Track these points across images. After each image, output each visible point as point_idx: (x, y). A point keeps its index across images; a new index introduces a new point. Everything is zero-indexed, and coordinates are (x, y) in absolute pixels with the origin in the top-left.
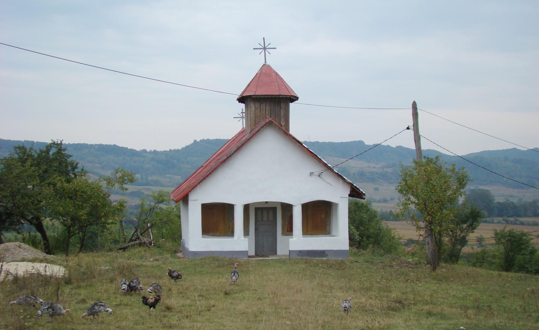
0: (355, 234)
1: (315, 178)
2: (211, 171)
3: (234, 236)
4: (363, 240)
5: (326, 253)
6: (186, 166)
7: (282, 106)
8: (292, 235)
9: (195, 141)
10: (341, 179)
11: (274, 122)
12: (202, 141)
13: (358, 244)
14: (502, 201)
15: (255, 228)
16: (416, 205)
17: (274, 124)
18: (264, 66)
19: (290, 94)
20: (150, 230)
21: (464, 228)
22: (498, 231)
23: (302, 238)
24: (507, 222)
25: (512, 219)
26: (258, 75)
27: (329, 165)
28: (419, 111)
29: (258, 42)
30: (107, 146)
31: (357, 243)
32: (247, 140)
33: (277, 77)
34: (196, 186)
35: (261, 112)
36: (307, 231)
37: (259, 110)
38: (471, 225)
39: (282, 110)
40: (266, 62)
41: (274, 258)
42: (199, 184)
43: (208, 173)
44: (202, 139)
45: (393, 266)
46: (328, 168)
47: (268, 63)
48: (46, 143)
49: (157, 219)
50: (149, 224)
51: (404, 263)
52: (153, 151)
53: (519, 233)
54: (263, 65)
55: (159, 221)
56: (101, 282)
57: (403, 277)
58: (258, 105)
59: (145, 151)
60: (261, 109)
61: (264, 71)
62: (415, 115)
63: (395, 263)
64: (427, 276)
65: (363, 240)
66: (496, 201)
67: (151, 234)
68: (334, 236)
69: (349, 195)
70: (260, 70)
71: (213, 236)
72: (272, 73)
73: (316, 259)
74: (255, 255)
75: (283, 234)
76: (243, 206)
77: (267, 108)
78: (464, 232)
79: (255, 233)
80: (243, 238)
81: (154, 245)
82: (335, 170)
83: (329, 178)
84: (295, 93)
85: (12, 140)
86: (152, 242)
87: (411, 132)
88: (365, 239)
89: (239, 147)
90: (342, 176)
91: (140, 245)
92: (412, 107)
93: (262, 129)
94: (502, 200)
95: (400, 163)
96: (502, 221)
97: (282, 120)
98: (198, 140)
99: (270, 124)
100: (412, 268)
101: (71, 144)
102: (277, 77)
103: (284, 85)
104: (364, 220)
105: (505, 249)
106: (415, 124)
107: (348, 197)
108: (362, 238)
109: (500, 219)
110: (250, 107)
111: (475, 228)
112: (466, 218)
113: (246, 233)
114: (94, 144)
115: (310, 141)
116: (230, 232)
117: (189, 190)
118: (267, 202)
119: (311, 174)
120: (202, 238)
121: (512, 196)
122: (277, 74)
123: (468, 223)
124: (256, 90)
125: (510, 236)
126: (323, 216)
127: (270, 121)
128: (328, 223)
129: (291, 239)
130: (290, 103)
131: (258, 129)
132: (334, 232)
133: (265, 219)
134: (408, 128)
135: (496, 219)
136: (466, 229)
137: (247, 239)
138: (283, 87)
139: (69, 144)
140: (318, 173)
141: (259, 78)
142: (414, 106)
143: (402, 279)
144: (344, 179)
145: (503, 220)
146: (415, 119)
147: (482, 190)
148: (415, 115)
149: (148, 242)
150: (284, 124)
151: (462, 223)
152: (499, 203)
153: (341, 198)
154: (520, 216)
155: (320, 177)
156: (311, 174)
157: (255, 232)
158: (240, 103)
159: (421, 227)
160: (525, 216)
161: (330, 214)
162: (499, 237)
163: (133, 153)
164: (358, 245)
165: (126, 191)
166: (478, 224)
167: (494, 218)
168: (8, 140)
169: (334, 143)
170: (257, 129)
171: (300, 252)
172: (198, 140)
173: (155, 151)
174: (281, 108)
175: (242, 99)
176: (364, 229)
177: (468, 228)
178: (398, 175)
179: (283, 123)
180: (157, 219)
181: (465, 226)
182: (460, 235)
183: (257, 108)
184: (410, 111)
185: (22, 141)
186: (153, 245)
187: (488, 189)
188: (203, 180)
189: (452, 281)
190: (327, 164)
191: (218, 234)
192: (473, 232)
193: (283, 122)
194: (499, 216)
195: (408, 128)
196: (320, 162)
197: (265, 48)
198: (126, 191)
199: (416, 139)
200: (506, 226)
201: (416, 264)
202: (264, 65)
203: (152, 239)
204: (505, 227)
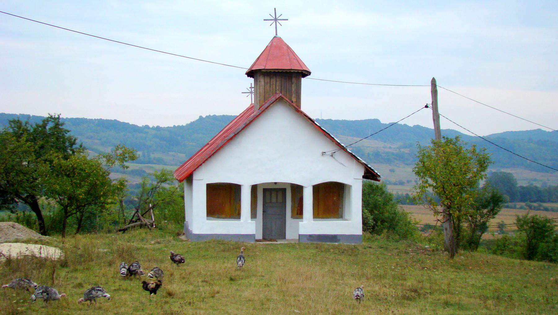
1: (327, 158)
5: (338, 238)
6: (191, 144)
8: (302, 218)
9: (201, 117)
12: (209, 117)
14: (525, 185)
15: (263, 210)
17: (285, 101)
19: (302, 68)
22: (521, 217)
24: (530, 207)
25: (535, 204)
26: (268, 48)
27: (342, 145)
28: (438, 88)
29: (268, 13)
30: (107, 120)
32: (255, 117)
33: (289, 50)
34: (201, 165)
35: (271, 87)
36: (318, 214)
37: (269, 84)
38: (492, 210)
39: (293, 85)
40: (276, 35)
42: (204, 162)
44: (208, 115)
47: (279, 35)
49: (160, 199)
50: (150, 204)
52: (156, 127)
55: (161, 202)
58: (267, 79)
59: (147, 127)
60: (271, 84)
61: (275, 44)
62: (434, 92)
63: (410, 250)
66: (518, 185)
68: (346, 220)
70: (270, 43)
71: (218, 218)
72: (283, 46)
73: (327, 244)
75: (293, 217)
76: (251, 187)
79: (263, 216)
80: (249, 220)
81: (155, 227)
82: (348, 150)
83: (341, 157)
87: (430, 111)
90: (356, 156)
91: (141, 226)
93: (272, 105)
94: (524, 184)
96: (525, 207)
97: (293, 96)
98: (204, 117)
102: (289, 50)
103: (294, 58)
105: (528, 236)
108: (377, 222)
109: (523, 204)
111: (496, 214)
112: (487, 203)
113: (254, 215)
116: (236, 214)
117: (194, 169)
118: (276, 183)
119: (323, 153)
120: (207, 220)
121: (535, 180)
122: (288, 47)
123: (489, 208)
124: (266, 64)
125: (533, 222)
127: (281, 96)
128: (340, 206)
129: (300, 223)
133: (274, 200)
134: (426, 107)
136: (486, 214)
138: (295, 61)
139: (67, 118)
140: (330, 153)
141: (269, 51)
142: (434, 83)
144: (358, 159)
145: (526, 205)
148: (434, 92)
149: (149, 224)
151: (483, 208)
152: (522, 187)
154: (544, 201)
156: (323, 153)
157: (263, 214)
158: (249, 77)
160: (549, 201)
161: (342, 197)
162: (521, 223)
163: (134, 128)
170: (266, 105)
172: (204, 117)
173: (158, 127)
174: (292, 83)
175: (251, 74)
176: (378, 213)
177: (488, 213)
178: (416, 156)
179: (294, 100)
180: (160, 199)
181: (485, 211)
182: (480, 221)
183: (267, 83)
184: (429, 89)
186: (154, 226)
187: (511, 172)
188: (208, 158)
189: (471, 269)
191: (224, 216)
192: (494, 218)
194: (522, 200)
195: (426, 107)
196: (333, 141)
197: (276, 20)
199: (435, 118)
201: (433, 251)
202: (275, 37)
203: (153, 220)
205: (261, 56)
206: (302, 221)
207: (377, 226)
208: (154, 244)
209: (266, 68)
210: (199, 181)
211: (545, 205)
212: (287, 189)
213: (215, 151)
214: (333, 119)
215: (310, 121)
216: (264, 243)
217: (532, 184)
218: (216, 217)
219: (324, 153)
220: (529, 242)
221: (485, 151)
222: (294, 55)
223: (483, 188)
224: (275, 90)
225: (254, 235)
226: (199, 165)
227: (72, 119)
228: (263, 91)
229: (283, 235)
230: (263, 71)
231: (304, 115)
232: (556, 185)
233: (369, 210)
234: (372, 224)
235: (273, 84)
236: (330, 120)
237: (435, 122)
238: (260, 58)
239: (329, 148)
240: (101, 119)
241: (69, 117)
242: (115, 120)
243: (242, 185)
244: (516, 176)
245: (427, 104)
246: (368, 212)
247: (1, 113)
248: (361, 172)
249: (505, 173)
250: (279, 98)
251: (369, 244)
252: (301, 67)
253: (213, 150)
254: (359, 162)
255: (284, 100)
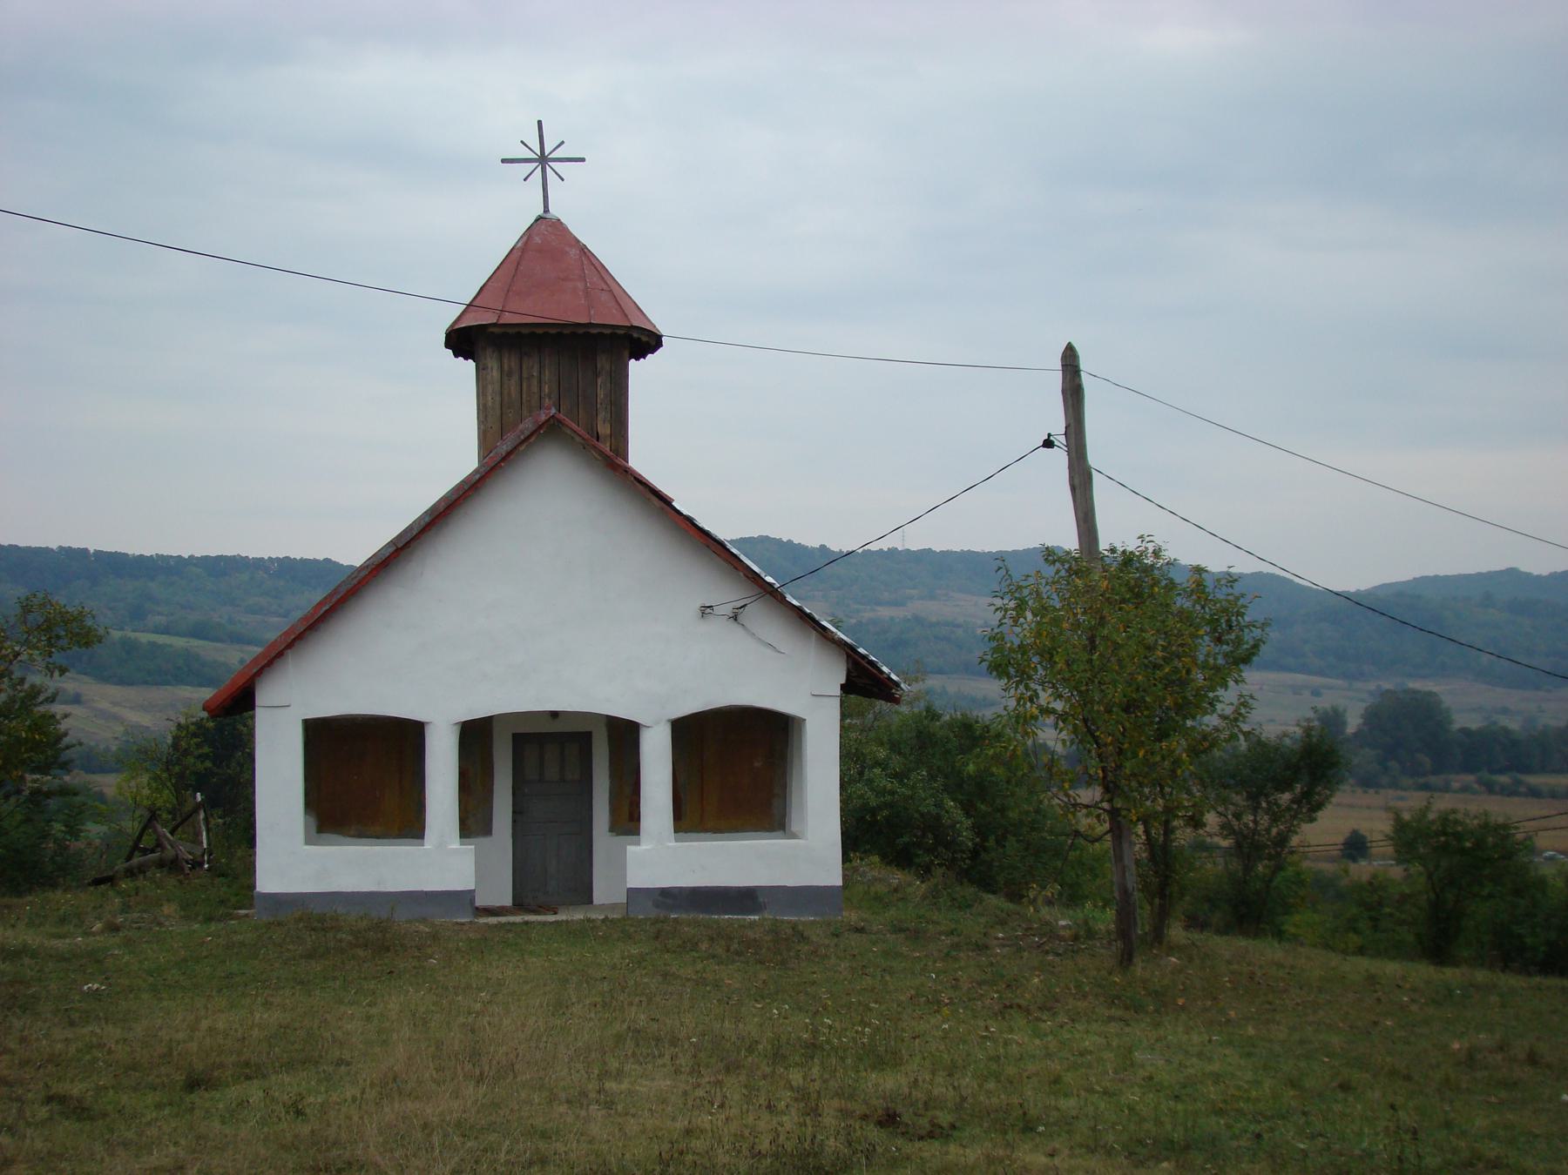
0: (958, 826)
1: (718, 627)
2: (334, 600)
3: (493, 832)
4: (987, 844)
7: (599, 366)
8: (638, 833)
10: (814, 628)
11: (568, 421)
13: (969, 858)
14: (1474, 726)
15: (513, 805)
16: (1057, 718)
17: (569, 432)
18: (539, 222)
19: (629, 320)
20: (202, 815)
21: (1283, 807)
22: (1406, 816)
23: (673, 844)
24: (1490, 788)
25: (1504, 779)
26: (517, 254)
27: (769, 579)
28: (1086, 380)
29: (516, 136)
30: (304, 562)
31: (964, 856)
32: (466, 487)
33: (585, 262)
34: (280, 654)
37: (515, 378)
38: (1307, 795)
39: (599, 381)
40: (546, 210)
41: (463, 921)
42: (290, 646)
43: (325, 609)
45: (987, 947)
46: (765, 590)
47: (555, 211)
48: (124, 554)
51: (1034, 935)
53: (1476, 822)
54: (537, 220)
56: (482, 952)
57: (997, 992)
58: (511, 361)
60: (525, 375)
62: (1073, 394)
63: (1001, 935)
64: (1087, 989)
65: (987, 844)
66: (1456, 726)
67: (203, 828)
68: (794, 836)
69: (842, 686)
70: (525, 238)
72: (567, 249)
74: (514, 904)
77: (547, 372)
78: (1283, 820)
79: (513, 829)
80: (455, 843)
81: (209, 870)
82: (789, 598)
83: (767, 625)
84: (649, 321)
85: (21, 544)
86: (206, 858)
87: (1059, 458)
88: (991, 842)
89: (437, 513)
90: (817, 617)
92: (1062, 365)
93: (522, 448)
94: (1474, 723)
95: (1001, 565)
96: (1476, 786)
97: (600, 417)
99: (550, 431)
100: (1058, 955)
101: (197, 557)
102: (585, 262)
103: (605, 287)
104: (989, 779)
105: (1430, 877)
106: (1072, 425)
107: (838, 692)
108: (985, 839)
109: (1469, 778)
110: (483, 369)
111: (1319, 806)
112: (1289, 773)
113: (473, 821)
114: (266, 558)
115: (907, 547)
116: (410, 825)
117: (255, 670)
118: (555, 714)
119: (706, 611)
121: (1505, 711)
122: (584, 251)
123: (1298, 787)
125: (1444, 833)
126: (757, 764)
129: (630, 848)
130: (632, 362)
131: (510, 448)
132: (794, 827)
134: (1048, 444)
135: (1457, 780)
136: (1288, 809)
137: (473, 847)
138: (604, 297)
139: (191, 557)
140: (728, 610)
141: (518, 264)
142: (1070, 361)
143: (988, 1001)
144: (825, 628)
145: (1479, 782)
146: (1071, 410)
147: (1415, 692)
148: (1073, 394)
149: (191, 857)
150: (608, 432)
151: (1277, 790)
152: (1465, 732)
153: (814, 698)
154: (1528, 770)
155: (739, 623)
156: (706, 611)
157: (514, 821)
158: (461, 359)
159: (1079, 801)
160: (1543, 769)
162: (1408, 838)
164: (967, 861)
165: (61, 675)
166: (1328, 793)
167: (216, 691)
168: (10, 545)
169: (978, 552)
171: (665, 892)
174: (596, 375)
175: (461, 341)
176: (990, 810)
177: (1295, 806)
178: (993, 608)
179: (604, 429)
181: (1285, 798)
182: (1268, 830)
183: (510, 374)
184: (1056, 380)
185: (52, 550)
186: (206, 866)
187: (1435, 689)
189: (1183, 1008)
190: (763, 576)
192: (1312, 820)
193: (604, 422)
194: (1467, 768)
195: (1048, 444)
196: (736, 568)
197: (543, 160)
198: (61, 675)
199: (1076, 481)
200: (1432, 800)
201: (1076, 938)
202: (539, 218)
204: (1429, 803)
205: (490, 283)
206: (638, 843)
207: (986, 850)
208: (102, 932)
209: (501, 322)
210: (282, 710)
211: (1533, 780)
212: (594, 735)
213: (327, 607)
214: (938, 547)
215: (654, 499)
216: (518, 919)
217: (1495, 723)
218: (352, 832)
219: (708, 610)
220: (1433, 896)
221: (1235, 585)
222: (603, 278)
223: (1355, 734)
224: (536, 396)
225: (472, 892)
226: (273, 655)
227: (206, 558)
228: (498, 399)
229: (582, 892)
230: (491, 330)
231: (635, 478)
232: (1562, 724)
233: (961, 803)
234: (970, 844)
235: (531, 376)
236: (928, 552)
237: (1078, 495)
238: (487, 287)
239: (726, 594)
240: (287, 557)
241: (198, 555)
242: (327, 560)
243: (427, 723)
244: (1447, 701)
245: (1049, 435)
246: (956, 808)
247: (6, 543)
248: (833, 676)
249: (1419, 692)
250: (549, 419)
251: (865, 916)
252: (626, 316)
253: (321, 604)
254: (825, 637)
255: (564, 429)
